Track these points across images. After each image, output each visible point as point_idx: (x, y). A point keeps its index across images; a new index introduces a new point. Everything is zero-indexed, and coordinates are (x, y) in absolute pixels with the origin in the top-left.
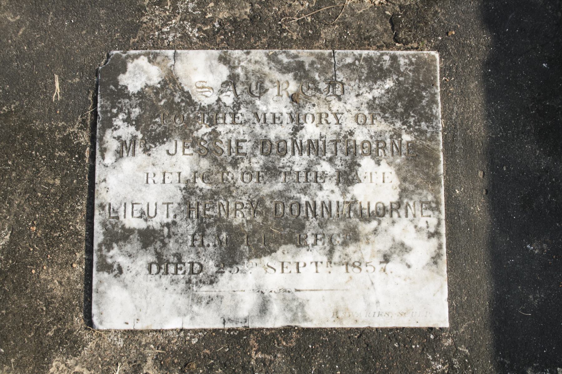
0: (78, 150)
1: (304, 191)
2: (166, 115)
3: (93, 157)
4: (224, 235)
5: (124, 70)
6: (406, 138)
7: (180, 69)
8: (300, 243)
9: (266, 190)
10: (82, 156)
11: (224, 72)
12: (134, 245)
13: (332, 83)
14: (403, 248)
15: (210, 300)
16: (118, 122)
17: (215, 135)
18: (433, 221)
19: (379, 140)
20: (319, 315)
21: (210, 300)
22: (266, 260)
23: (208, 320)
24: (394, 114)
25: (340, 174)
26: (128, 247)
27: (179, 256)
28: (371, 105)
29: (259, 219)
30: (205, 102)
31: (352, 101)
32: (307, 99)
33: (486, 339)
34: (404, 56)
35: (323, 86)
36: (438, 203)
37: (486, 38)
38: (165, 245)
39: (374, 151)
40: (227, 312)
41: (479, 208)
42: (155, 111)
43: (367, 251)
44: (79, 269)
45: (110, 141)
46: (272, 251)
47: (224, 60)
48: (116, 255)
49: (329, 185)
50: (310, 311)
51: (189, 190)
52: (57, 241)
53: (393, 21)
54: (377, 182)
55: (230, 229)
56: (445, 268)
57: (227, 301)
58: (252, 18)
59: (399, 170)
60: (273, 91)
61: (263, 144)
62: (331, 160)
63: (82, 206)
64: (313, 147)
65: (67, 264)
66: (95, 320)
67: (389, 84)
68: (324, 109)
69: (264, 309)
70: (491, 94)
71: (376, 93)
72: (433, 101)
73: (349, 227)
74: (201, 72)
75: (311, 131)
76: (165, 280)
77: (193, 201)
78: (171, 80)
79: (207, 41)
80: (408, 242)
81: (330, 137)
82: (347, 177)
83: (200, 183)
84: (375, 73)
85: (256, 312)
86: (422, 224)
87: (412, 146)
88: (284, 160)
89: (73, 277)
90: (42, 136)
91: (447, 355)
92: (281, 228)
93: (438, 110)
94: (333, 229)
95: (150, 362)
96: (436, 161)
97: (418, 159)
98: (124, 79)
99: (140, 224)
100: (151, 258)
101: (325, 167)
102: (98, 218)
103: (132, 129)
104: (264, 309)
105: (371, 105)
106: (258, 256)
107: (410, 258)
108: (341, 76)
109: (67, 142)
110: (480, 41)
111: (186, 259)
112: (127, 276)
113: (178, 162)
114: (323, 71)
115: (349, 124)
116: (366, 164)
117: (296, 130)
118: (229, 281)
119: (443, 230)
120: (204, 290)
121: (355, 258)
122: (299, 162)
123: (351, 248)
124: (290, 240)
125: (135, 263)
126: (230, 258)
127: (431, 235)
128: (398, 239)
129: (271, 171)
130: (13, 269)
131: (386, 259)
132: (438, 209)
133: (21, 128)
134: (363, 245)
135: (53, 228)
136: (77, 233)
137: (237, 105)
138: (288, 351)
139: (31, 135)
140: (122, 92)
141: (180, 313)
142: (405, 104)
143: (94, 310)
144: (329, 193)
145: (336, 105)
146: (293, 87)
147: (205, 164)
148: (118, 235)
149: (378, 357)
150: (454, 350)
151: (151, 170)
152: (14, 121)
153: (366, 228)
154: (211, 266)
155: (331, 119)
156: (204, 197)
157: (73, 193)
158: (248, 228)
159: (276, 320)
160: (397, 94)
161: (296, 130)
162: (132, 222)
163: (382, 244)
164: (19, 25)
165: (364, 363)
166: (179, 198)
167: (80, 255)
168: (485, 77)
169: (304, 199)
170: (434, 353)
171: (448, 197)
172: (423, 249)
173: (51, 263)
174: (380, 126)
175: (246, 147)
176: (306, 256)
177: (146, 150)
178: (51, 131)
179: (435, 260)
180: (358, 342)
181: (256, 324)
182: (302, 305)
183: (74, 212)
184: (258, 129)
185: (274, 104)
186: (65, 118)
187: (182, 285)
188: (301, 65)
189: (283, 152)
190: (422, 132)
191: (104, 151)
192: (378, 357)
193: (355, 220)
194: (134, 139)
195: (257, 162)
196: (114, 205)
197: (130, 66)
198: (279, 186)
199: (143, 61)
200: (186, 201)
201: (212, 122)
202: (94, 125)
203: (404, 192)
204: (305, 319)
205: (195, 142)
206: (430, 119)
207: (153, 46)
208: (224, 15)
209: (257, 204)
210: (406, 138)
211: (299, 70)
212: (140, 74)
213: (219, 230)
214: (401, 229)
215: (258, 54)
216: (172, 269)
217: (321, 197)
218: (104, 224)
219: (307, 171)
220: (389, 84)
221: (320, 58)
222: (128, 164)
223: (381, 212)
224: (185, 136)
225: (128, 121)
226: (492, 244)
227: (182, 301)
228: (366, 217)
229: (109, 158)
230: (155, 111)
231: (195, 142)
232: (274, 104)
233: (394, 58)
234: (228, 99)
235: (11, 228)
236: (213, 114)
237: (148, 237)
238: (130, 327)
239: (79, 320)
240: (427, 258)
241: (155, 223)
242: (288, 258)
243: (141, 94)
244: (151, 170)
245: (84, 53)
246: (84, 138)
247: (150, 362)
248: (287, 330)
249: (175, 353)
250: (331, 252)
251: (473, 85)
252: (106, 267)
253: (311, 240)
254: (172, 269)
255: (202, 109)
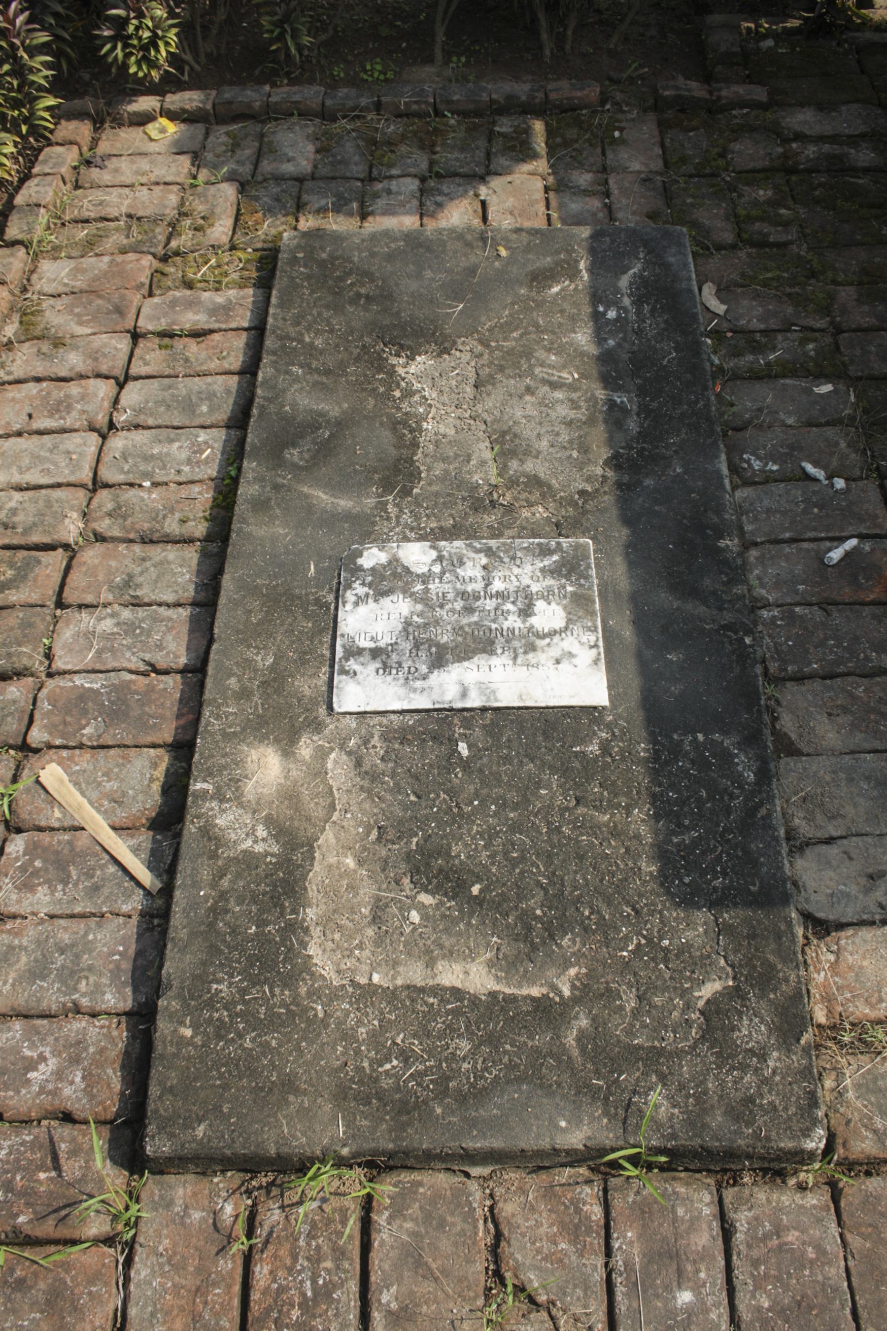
0: (327, 606)
1: (494, 621)
2: (391, 580)
3: (337, 608)
4: (434, 649)
5: (361, 556)
6: (570, 589)
7: (401, 554)
8: (492, 653)
9: (465, 621)
10: (328, 609)
11: (434, 554)
12: (367, 657)
13: (513, 558)
14: (571, 655)
15: (423, 690)
16: (356, 585)
17: (427, 590)
18: (593, 638)
19: (550, 590)
20: (507, 698)
21: (423, 690)
22: (466, 664)
23: (422, 702)
24: (560, 575)
25: (520, 610)
26: (362, 659)
27: (400, 664)
28: (542, 570)
29: (460, 639)
30: (420, 571)
31: (528, 568)
32: (495, 568)
33: (639, 717)
34: (565, 542)
35: (506, 560)
36: (596, 628)
37: (625, 531)
38: (389, 657)
39: (547, 595)
40: (435, 697)
41: (628, 633)
42: (383, 578)
43: (544, 657)
44: (324, 678)
45: (350, 596)
46: (470, 658)
47: (433, 547)
48: (352, 664)
49: (511, 618)
50: (499, 695)
51: (407, 623)
52: (309, 661)
53: (557, 525)
54: (549, 615)
55: (438, 645)
56: (604, 668)
57: (436, 690)
58: (454, 526)
59: (565, 608)
60: (469, 564)
61: (463, 595)
62: (513, 603)
63: (327, 639)
64: (501, 595)
65: (315, 675)
66: (335, 706)
67: (555, 558)
68: (507, 573)
69: (464, 694)
70: (632, 565)
71: (546, 563)
72: (589, 567)
73: (528, 643)
74: (417, 555)
75: (498, 585)
76: (389, 679)
77: (411, 629)
78: (394, 561)
79: (421, 538)
80: (574, 652)
81: (512, 589)
82: (526, 612)
83: (415, 618)
84: (545, 551)
85: (458, 695)
86: (584, 639)
87: (573, 594)
88: (478, 603)
89: (319, 683)
90: (300, 598)
91: (609, 727)
92: (478, 643)
93: (593, 572)
94: (516, 644)
95: (376, 738)
96: (594, 602)
97: (579, 604)
98: (360, 561)
99: (372, 645)
100: (378, 665)
101: (509, 606)
102: (339, 642)
103: (366, 589)
104: (464, 694)
105: (542, 570)
106: (459, 661)
107: (575, 661)
108: (519, 554)
109: (317, 601)
110: (622, 533)
111: (405, 665)
112: (360, 677)
113: (399, 607)
114: (506, 552)
115: (526, 581)
116: (540, 605)
117: (487, 586)
118: (436, 678)
119: (601, 643)
120: (419, 684)
121: (533, 661)
122: (490, 604)
123: (530, 656)
124: (484, 651)
125: (367, 670)
126: (438, 662)
127: (591, 647)
128: (567, 649)
129: (469, 610)
130: (275, 680)
131: (558, 662)
132: (596, 630)
133: (285, 594)
134: (539, 653)
135: (305, 653)
136: (323, 655)
137: (443, 573)
138: (484, 727)
139: (292, 598)
140: (360, 568)
141: (399, 699)
142: (570, 568)
143: (335, 699)
144: (513, 622)
145: (516, 571)
146: (484, 561)
147: (419, 607)
148: (354, 652)
149: (554, 729)
150: (615, 722)
151: (379, 612)
152: (281, 589)
153: (541, 643)
154: (424, 669)
155: (513, 578)
156: (418, 627)
157: (321, 631)
158: (451, 645)
159: (474, 701)
160: (562, 564)
161: (487, 586)
162: (365, 643)
163: (555, 652)
164: (287, 535)
165: (544, 733)
166: (400, 627)
167: (325, 669)
168: (627, 554)
169: (494, 626)
170: (599, 725)
171: (604, 622)
172: (586, 656)
173: (303, 675)
174: (549, 582)
175: (450, 596)
176: (495, 661)
177: (376, 601)
178: (307, 595)
179: (596, 662)
180: (539, 720)
181: (459, 705)
182: (494, 692)
183: (321, 642)
184: (458, 586)
185: (472, 570)
186: (317, 587)
187: (402, 681)
188: (490, 549)
189: (477, 598)
190: (581, 585)
191: (344, 603)
192: (554, 729)
193: (533, 638)
194: (367, 595)
195: (459, 605)
196: (352, 634)
197: (365, 554)
198: (475, 618)
199: (375, 550)
200: (405, 630)
201: (424, 583)
202: (338, 590)
203: (569, 621)
204: (496, 700)
205: (412, 595)
206: (587, 577)
207: (382, 542)
208: (434, 525)
209: (458, 630)
210: (570, 589)
211: (489, 552)
212: (372, 557)
213: (430, 647)
214: (569, 643)
215: (458, 543)
216: (394, 671)
217: (506, 625)
218: (344, 646)
219: (496, 609)
220: (555, 558)
221: (504, 544)
222: (362, 609)
223: (552, 634)
224: (404, 592)
225: (363, 584)
226: (639, 655)
227: (402, 691)
228: (542, 636)
229: (349, 607)
230: (383, 578)
231: (412, 595)
232: (472, 570)
233: (558, 544)
234: (437, 569)
235: (275, 655)
236: (425, 578)
237: (375, 653)
238: (362, 709)
239: (322, 711)
240: (589, 661)
241: (382, 644)
242: (483, 662)
243: (373, 569)
244: (379, 612)
245: (332, 549)
246: (331, 598)
247: (376, 738)
248: (484, 709)
249: (395, 731)
250: (515, 658)
251: (619, 559)
252: (344, 672)
253: (499, 651)
254: (394, 671)
255: (418, 576)
